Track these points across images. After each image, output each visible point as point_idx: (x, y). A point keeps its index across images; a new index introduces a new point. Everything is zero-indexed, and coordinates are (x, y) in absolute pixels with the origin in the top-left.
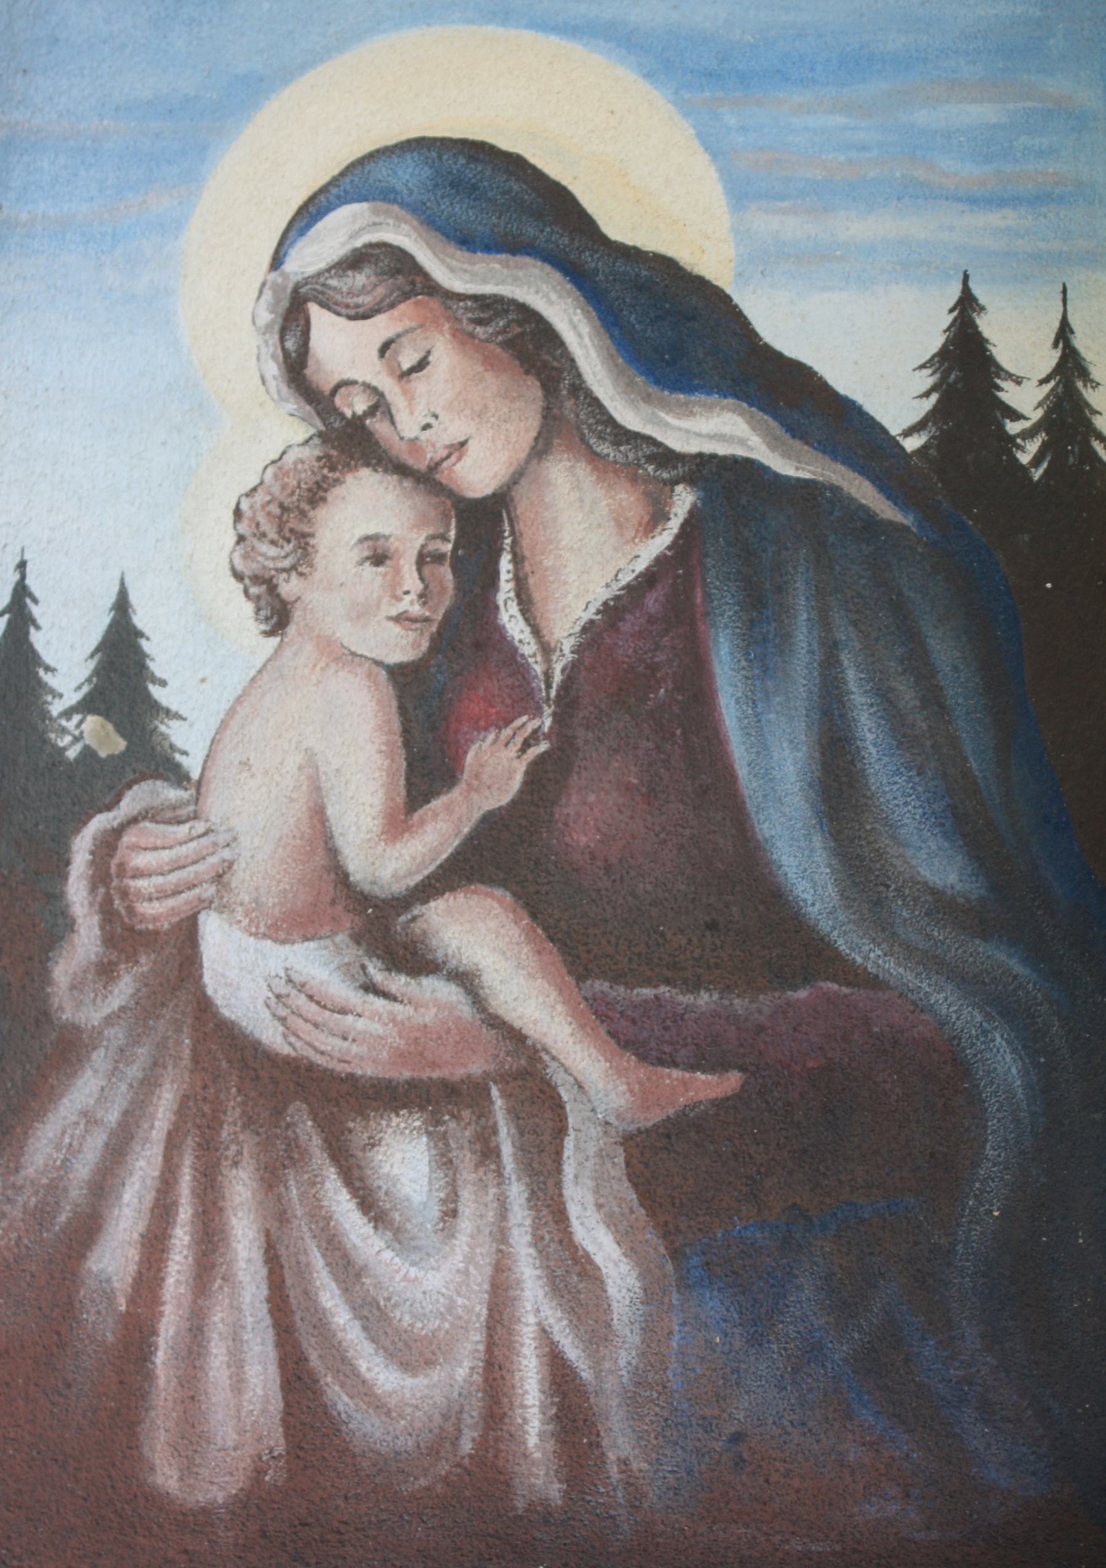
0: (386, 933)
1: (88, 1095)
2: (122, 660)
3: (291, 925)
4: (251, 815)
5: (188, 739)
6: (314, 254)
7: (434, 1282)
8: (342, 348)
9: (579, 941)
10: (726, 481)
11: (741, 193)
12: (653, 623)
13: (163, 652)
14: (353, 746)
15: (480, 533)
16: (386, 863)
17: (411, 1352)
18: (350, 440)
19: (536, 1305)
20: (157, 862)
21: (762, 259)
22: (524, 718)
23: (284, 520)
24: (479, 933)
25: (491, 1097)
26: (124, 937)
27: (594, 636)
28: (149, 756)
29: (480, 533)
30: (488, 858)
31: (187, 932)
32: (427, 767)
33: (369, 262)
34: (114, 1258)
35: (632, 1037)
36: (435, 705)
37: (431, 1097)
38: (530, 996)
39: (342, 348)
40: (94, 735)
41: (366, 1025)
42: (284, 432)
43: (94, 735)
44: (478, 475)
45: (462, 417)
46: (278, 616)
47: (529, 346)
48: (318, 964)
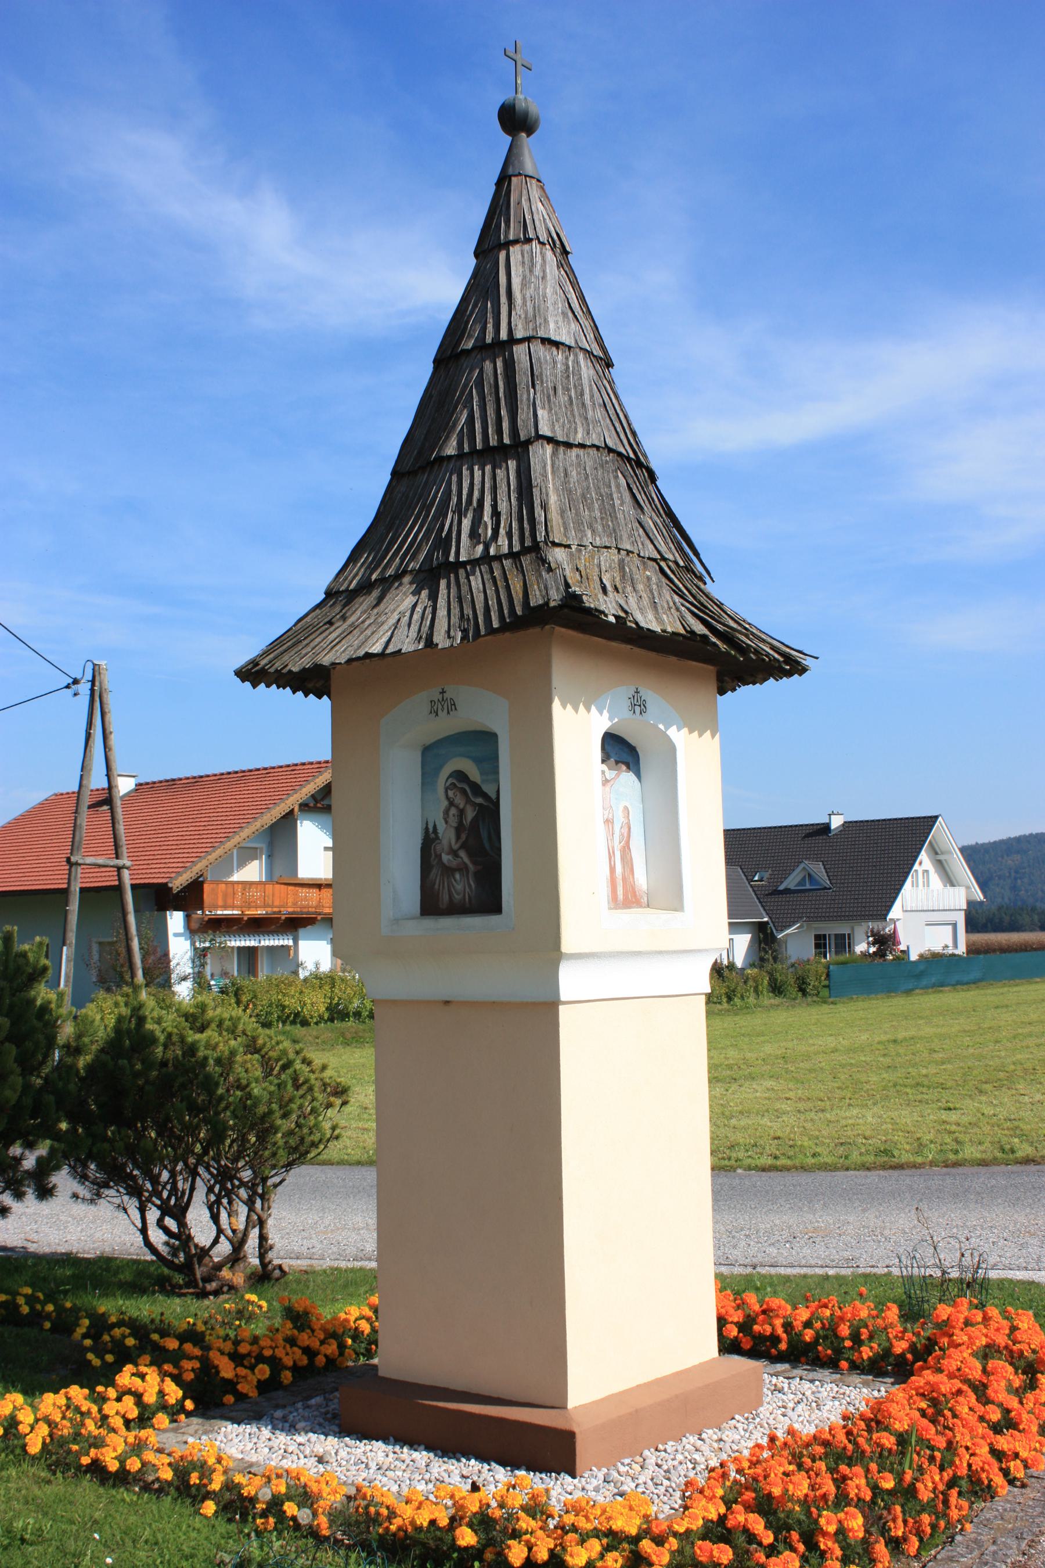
0: (454, 853)
1: (434, 871)
2: (435, 827)
3: (448, 854)
4: (445, 842)
5: (440, 835)
6: (448, 784)
7: (459, 887)
8: (451, 793)
9: (470, 855)
10: (480, 805)
11: (481, 774)
12: (475, 820)
13: (438, 827)
14: (452, 835)
15: (462, 812)
16: (455, 847)
17: (458, 894)
18: (451, 804)
19: (467, 890)
20: (438, 848)
21: (483, 781)
22: (352, 587)
23: (446, 812)
24: (462, 854)
25: (463, 869)
26: (436, 855)
27: (471, 822)
28: (437, 838)
29: (462, 812)
30: (463, 846)
31: (441, 855)
32: (458, 837)
33: (454, 1540)
34: (436, 886)
35: (474, 863)
36: (459, 829)
37: (459, 870)
38: (466, 860)
39: (451, 793)
40: (433, 836)
41: (454, 863)
42: (446, 803)
43: (433, 836)
44: (461, 806)
45: (460, 801)
46: (446, 822)
47: (463, 792)
48: (450, 857)
